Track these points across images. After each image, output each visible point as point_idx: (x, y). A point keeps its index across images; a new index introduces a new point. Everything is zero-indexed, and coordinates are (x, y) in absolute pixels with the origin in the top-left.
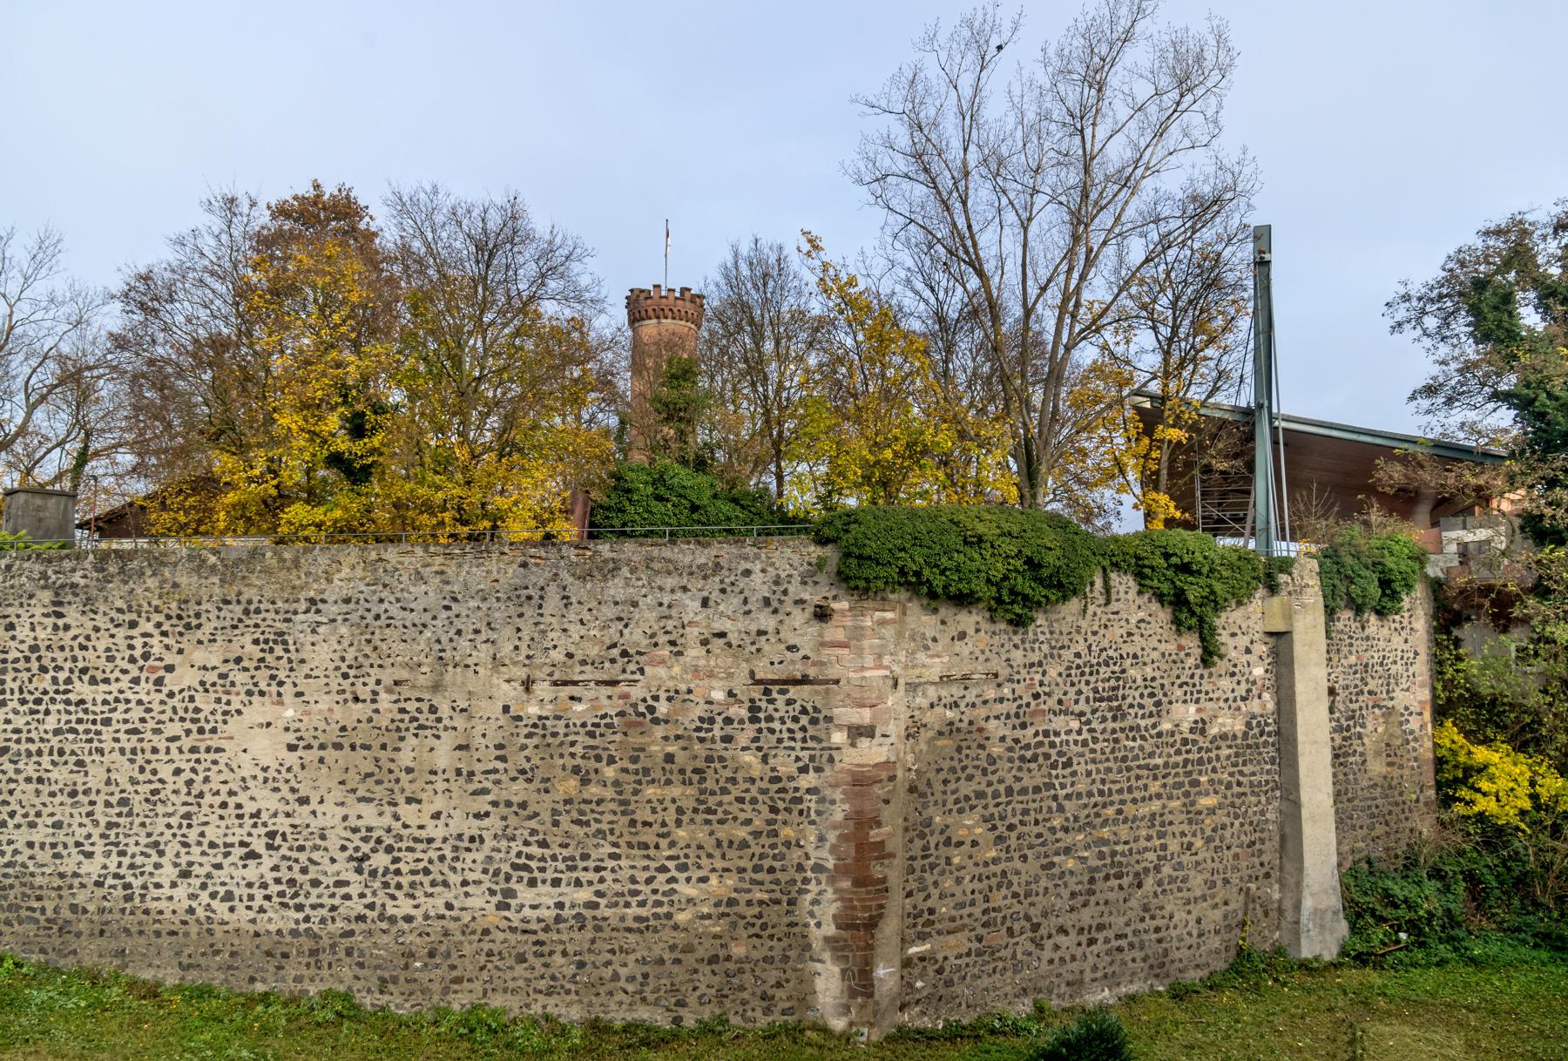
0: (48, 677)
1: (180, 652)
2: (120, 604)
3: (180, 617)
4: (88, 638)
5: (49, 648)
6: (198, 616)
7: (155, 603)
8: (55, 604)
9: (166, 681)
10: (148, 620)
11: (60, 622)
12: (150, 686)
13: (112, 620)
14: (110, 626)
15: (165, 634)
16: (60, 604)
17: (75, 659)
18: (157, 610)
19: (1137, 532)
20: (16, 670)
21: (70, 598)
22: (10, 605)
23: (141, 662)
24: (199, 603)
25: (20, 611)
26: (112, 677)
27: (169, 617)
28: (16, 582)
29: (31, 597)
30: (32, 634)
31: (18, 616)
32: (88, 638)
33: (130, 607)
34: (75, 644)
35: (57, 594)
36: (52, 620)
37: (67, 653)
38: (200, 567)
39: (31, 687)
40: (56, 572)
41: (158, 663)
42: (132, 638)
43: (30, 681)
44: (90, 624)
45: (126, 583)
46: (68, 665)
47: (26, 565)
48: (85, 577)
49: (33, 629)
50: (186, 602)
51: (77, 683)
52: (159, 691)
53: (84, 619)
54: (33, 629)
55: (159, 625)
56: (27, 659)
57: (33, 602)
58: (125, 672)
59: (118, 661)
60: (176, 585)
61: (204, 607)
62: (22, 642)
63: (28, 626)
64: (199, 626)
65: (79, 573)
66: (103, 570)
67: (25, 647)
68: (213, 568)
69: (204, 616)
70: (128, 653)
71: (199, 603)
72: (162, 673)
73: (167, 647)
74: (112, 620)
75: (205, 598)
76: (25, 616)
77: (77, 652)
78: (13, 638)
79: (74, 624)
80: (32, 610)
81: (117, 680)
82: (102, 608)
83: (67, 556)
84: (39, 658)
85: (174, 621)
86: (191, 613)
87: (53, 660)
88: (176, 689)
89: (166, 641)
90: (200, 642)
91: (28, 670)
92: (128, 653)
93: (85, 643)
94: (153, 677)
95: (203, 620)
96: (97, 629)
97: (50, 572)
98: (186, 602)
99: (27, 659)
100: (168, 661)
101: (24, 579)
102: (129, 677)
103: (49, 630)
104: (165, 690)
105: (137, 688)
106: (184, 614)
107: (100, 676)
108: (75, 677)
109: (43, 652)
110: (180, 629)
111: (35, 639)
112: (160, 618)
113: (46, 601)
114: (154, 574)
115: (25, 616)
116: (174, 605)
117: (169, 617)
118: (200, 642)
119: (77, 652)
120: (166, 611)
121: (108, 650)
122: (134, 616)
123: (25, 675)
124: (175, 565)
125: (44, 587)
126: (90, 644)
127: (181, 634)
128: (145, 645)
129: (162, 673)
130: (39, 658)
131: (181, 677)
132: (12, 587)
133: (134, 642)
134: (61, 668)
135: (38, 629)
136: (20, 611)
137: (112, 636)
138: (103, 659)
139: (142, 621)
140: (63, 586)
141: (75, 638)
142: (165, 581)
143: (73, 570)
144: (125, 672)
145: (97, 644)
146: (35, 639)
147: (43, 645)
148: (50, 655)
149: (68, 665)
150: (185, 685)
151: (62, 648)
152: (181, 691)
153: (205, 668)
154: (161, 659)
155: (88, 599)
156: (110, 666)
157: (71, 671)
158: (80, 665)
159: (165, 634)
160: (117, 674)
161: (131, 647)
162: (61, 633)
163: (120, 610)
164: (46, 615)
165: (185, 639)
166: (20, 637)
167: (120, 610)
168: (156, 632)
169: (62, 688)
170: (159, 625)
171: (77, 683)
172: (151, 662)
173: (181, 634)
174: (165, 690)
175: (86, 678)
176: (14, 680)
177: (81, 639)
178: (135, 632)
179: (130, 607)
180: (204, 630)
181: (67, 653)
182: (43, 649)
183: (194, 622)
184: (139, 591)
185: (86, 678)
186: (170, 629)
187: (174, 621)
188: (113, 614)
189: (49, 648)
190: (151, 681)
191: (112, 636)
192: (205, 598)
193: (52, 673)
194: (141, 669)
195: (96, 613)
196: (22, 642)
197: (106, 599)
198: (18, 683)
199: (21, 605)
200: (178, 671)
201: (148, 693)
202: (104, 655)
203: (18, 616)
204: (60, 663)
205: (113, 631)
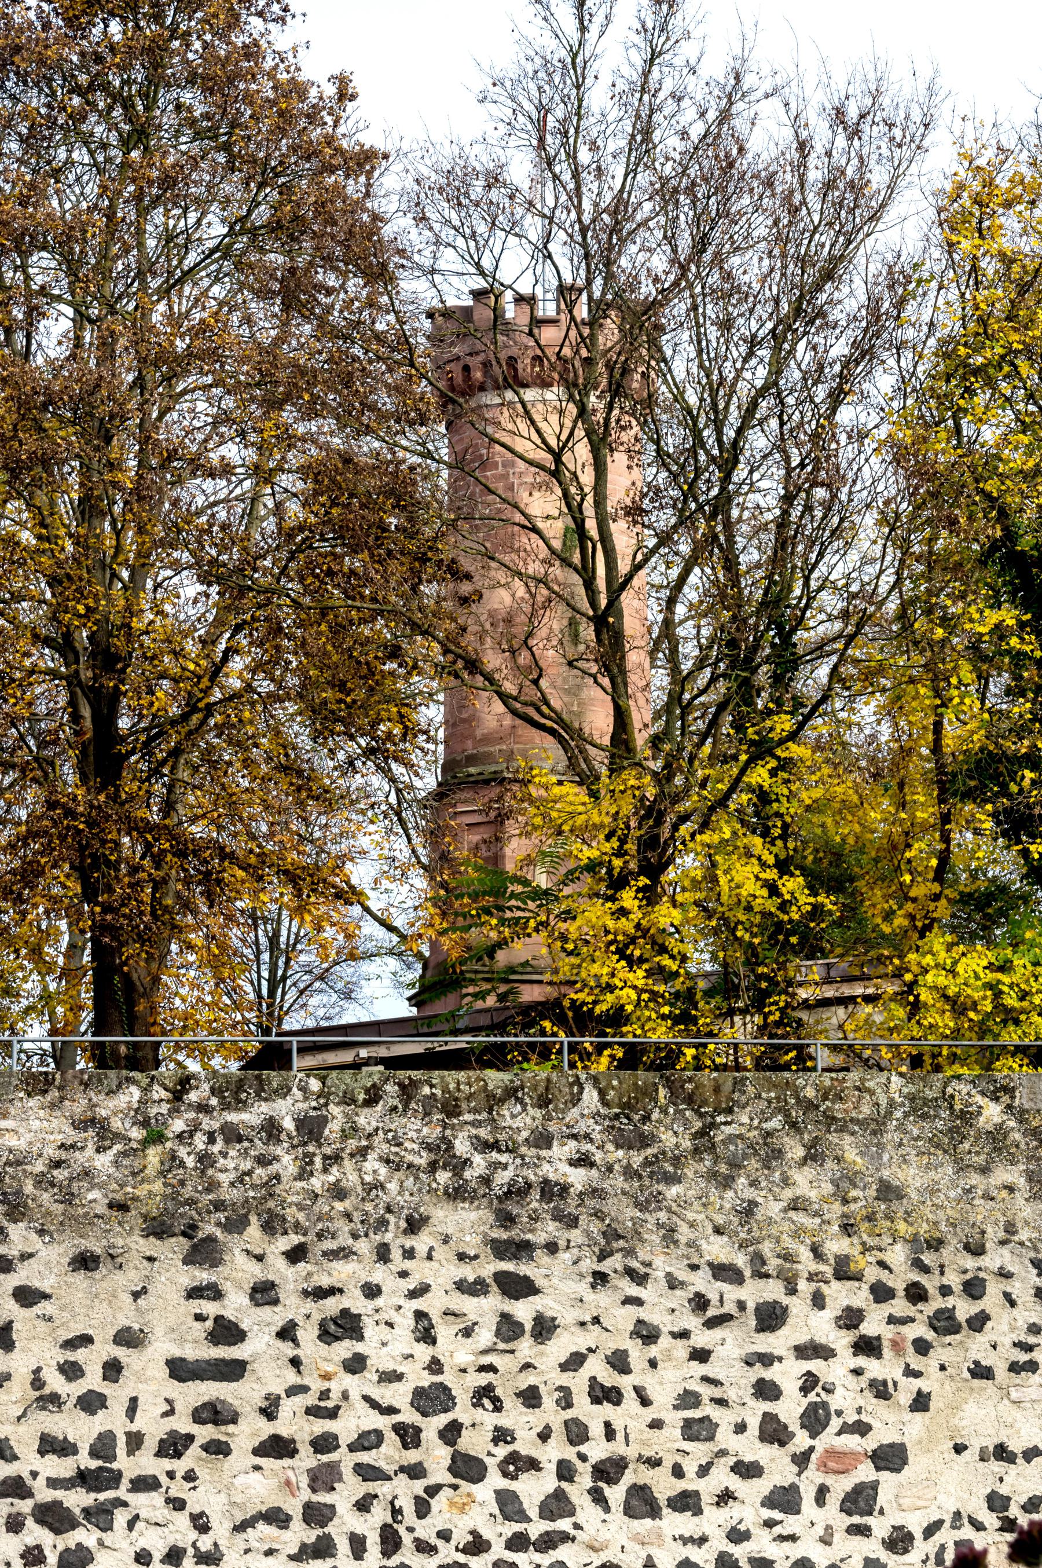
0: (485, 1492)
1: (921, 1403)
2: (718, 1250)
3: (916, 1294)
4: (619, 1362)
5: (485, 1395)
6: (974, 1288)
7: (836, 1246)
8: (501, 1249)
9: (883, 1498)
10: (818, 1301)
11: (523, 1310)
12: (832, 1514)
13: (700, 1303)
14: (692, 1322)
15: (868, 1347)
16: (522, 1249)
17: (577, 1433)
18: (844, 1272)
19: (55, 1438)
20: (367, 1473)
21: (548, 1229)
22: (343, 1254)
23: (802, 1440)
24: (977, 1250)
25: (380, 1275)
26: (708, 1488)
27: (881, 1293)
28: (349, 1174)
29: (414, 1225)
30: (423, 1353)
31: (372, 1291)
32: (619, 1362)
33: (758, 1259)
34: (578, 1382)
35: (507, 1220)
36: (493, 1303)
37: (550, 1413)
38: (956, 1134)
39: (426, 1530)
40: (485, 1146)
41: (852, 1442)
42: (767, 1360)
43: (422, 1509)
44: (624, 1318)
45: (726, 1183)
46: (555, 1451)
47: (367, 1119)
48: (583, 1161)
49: (426, 1336)
50: (936, 1244)
51: (587, 1512)
52: (862, 1531)
53: (603, 1300)
54: (426, 1336)
55: (851, 1318)
56: (409, 1436)
57: (421, 1243)
58: (748, 1470)
59: (725, 1437)
60: (888, 1192)
61: (995, 1258)
62: (392, 1377)
63: (406, 1322)
64: (978, 1322)
65: (563, 1150)
66: (644, 1141)
67: (399, 1395)
68: (997, 1137)
69: (994, 1289)
70: (754, 1412)
71: (977, 1250)
72: (865, 1472)
73: (881, 1390)
74: (700, 1303)
75: (994, 1233)
76: (394, 1289)
77: (583, 1408)
78: (356, 1365)
79: (567, 1316)
80: (420, 1271)
81: (725, 1497)
82: (662, 1264)
83: (511, 1093)
84: (451, 1433)
85: (900, 1306)
86: (953, 1280)
87: (502, 1435)
88: (916, 1525)
89: (874, 1368)
90: (981, 1372)
91: (415, 1472)
92: (754, 1412)
93: (608, 1377)
94: (841, 1486)
95: (991, 1301)
96: (647, 1334)
97: (462, 1146)
98: (936, 1244)
99: (409, 1436)
100: (881, 1436)
101: (371, 1163)
102: (762, 1486)
103: (485, 1336)
104: (881, 1527)
105: (791, 1524)
106: (930, 1283)
107: (664, 1486)
108: (578, 1492)
109: (463, 1412)
110: (919, 1330)
111: (435, 1366)
112: (859, 1296)
113: (472, 1243)
114: (813, 1156)
115: (394, 1289)
116: (898, 1255)
117: (881, 1293)
118: (981, 1372)
119: (583, 1408)
120: (872, 1274)
121: (688, 1399)
122: (773, 1291)
123: (405, 1491)
124: (876, 1125)
125: (457, 1194)
126: (625, 1383)
127: (922, 1347)
128: (810, 1382)
129: (865, 1472)
130: (451, 1433)
131: (931, 1481)
132: (339, 1192)
133: (773, 1373)
134: (533, 1465)
135: (444, 1332)
136: (380, 1275)
137: (701, 1355)
138: (673, 1432)
139: (798, 1306)
140: (517, 1192)
141: (574, 1362)
142: (852, 1178)
143: (543, 1140)
144: (748, 1470)
145: (650, 1382)
146: (435, 1366)
147: (462, 1389)
148: (489, 1419)
149: (555, 1451)
150: (944, 1508)
151: (531, 1397)
152: (930, 1531)
153: (1002, 1453)
154: (861, 1429)
155: (612, 1234)
156: (699, 1452)
157: (565, 1471)
158: (597, 1450)
159: (868, 1347)
160: (721, 1477)
161: (766, 1390)
162: (525, 1347)
163: (723, 1272)
164: (474, 1288)
165: (929, 1364)
166: (380, 1359)
167: (723, 1272)
168: (841, 1341)
169: (536, 1529)
170: (851, 1318)
171: (587, 1512)
172: (828, 1439)
173: (922, 1347)
174: (881, 1527)
175: (616, 1494)
176: (363, 1505)
177: (596, 1367)
178: (778, 1342)
179: (758, 1259)
180: (995, 1329)
181: (550, 1413)
182: (463, 1398)
183: (964, 1309)
184: (773, 1209)
185: (616, 1494)
186: (887, 1333)
187: (900, 1306)
188: (701, 1282)
189: (485, 1395)
190: (834, 1500)
191: (701, 1355)
192: (994, 1233)
193: (495, 1480)
194: (802, 1460)
195: (639, 1278)
196: (392, 1377)
197: (669, 1235)
198: (379, 1515)
199: (383, 1254)
200: (917, 1465)
201: (826, 1541)
202: (675, 1419)
203: (372, 1291)
204: (525, 1445)
205: (702, 1338)
